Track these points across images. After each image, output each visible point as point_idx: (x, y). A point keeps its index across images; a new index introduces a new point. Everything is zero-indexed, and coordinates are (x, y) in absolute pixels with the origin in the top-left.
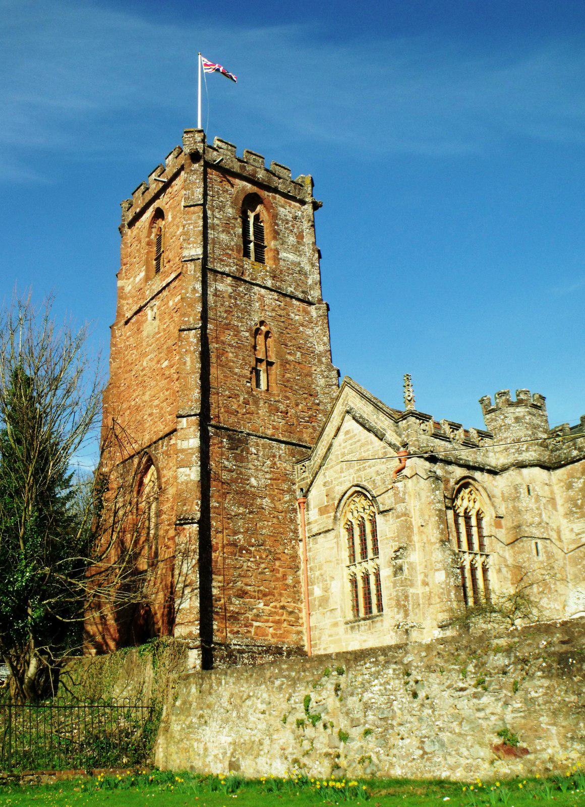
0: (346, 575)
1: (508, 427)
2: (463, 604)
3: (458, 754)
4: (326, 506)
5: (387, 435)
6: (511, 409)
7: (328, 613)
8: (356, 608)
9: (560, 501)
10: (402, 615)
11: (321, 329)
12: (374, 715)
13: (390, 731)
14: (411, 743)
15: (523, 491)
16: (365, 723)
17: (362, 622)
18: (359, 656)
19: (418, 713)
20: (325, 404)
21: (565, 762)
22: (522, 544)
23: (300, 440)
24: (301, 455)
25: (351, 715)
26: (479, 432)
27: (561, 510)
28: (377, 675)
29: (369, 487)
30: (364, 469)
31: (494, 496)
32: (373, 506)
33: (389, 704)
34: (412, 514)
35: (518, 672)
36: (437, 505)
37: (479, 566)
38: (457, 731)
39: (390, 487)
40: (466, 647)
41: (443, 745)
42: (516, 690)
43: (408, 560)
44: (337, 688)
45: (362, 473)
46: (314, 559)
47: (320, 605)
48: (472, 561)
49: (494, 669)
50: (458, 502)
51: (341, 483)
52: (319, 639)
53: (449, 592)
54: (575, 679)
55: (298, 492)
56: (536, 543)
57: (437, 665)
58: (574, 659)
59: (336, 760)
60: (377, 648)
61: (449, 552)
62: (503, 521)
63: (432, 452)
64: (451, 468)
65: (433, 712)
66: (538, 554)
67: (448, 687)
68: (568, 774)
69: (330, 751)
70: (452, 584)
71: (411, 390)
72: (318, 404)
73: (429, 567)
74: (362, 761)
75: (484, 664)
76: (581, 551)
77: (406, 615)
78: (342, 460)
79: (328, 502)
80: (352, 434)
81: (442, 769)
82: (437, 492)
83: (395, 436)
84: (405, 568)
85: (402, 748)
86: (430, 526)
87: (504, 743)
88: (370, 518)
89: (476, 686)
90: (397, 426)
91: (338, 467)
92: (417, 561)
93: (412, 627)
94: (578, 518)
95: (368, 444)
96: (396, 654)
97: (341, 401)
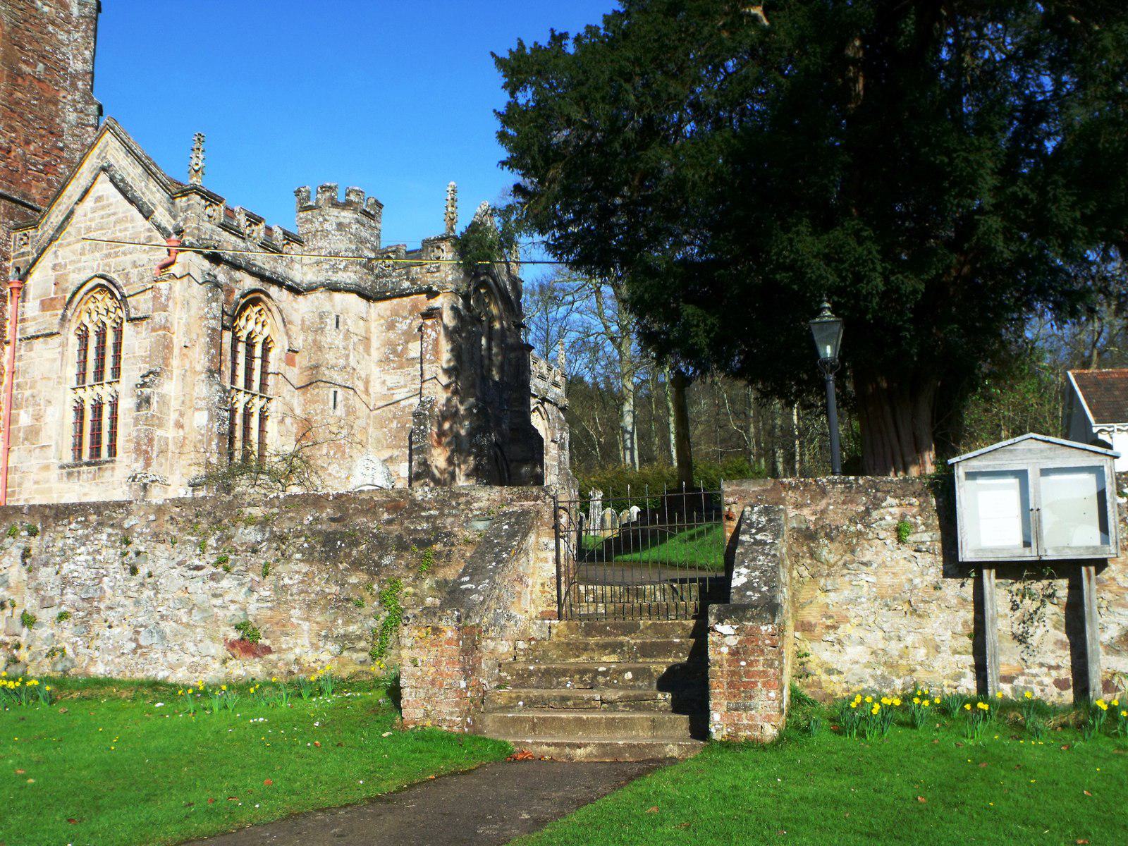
0: (70, 399)
1: (326, 234)
2: (226, 459)
3: (182, 650)
4: (52, 299)
5: (156, 213)
6: (335, 211)
7: (37, 450)
8: (78, 448)
9: (375, 343)
10: (141, 463)
11: (82, 37)
12: (75, 594)
13: (95, 616)
14: (121, 633)
15: (331, 322)
16: (61, 604)
17: (85, 468)
18: (61, 513)
19: (136, 595)
20: (72, 151)
21: (312, 665)
22: (317, 390)
23: (24, 196)
24: (23, 219)
25: (42, 593)
26: (285, 233)
27: (376, 354)
28: (84, 540)
29: (120, 281)
30: (116, 255)
31: (290, 322)
32: (121, 308)
33: (97, 581)
34: (175, 328)
35: (271, 552)
36: (211, 321)
37: (256, 411)
38: (184, 620)
39: (150, 286)
40: (209, 514)
41: (163, 637)
42: (266, 574)
43: (159, 390)
44: (26, 554)
45: (112, 261)
46: (25, 371)
47: (26, 439)
48: (248, 403)
49: (242, 545)
50: (242, 322)
51: (79, 270)
52: (20, 485)
53: (210, 441)
54: (341, 566)
55: (12, 272)
56: (335, 392)
57: (167, 533)
58: (343, 542)
59: (15, 651)
60: (88, 504)
61: (217, 387)
62: (297, 357)
63: (216, 248)
64: (238, 275)
65: (155, 594)
66: (335, 407)
67: (179, 564)
68: (312, 679)
69: (7, 639)
70: (215, 429)
71: (201, 156)
72: (61, 149)
73: (187, 402)
74: (52, 653)
75: (229, 538)
76: (390, 411)
77: (148, 464)
78: (85, 237)
79: (55, 294)
80: (105, 202)
81: (160, 667)
82: (214, 304)
83: (168, 217)
84: (154, 400)
85: (109, 638)
86: (197, 349)
87: (242, 639)
88: (115, 325)
89: (215, 565)
90: (173, 204)
91: (78, 246)
92: (172, 394)
93: (153, 481)
94: (394, 369)
95: (127, 221)
96: (114, 514)
97: (96, 151)
